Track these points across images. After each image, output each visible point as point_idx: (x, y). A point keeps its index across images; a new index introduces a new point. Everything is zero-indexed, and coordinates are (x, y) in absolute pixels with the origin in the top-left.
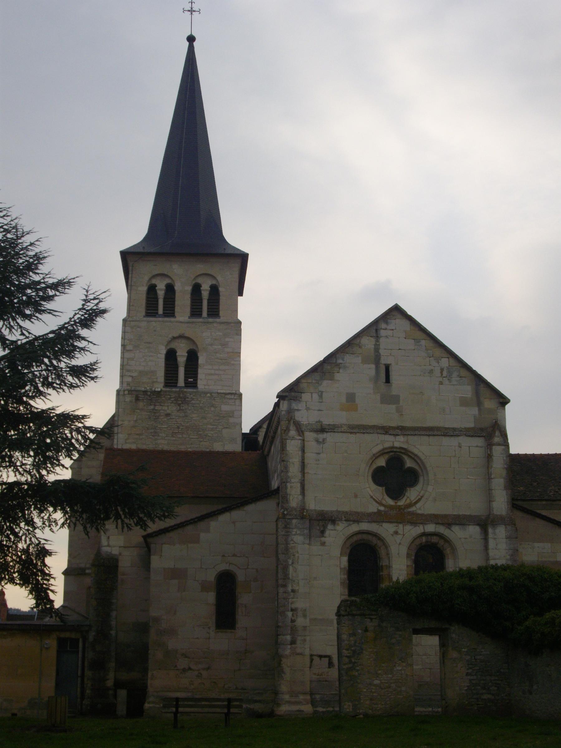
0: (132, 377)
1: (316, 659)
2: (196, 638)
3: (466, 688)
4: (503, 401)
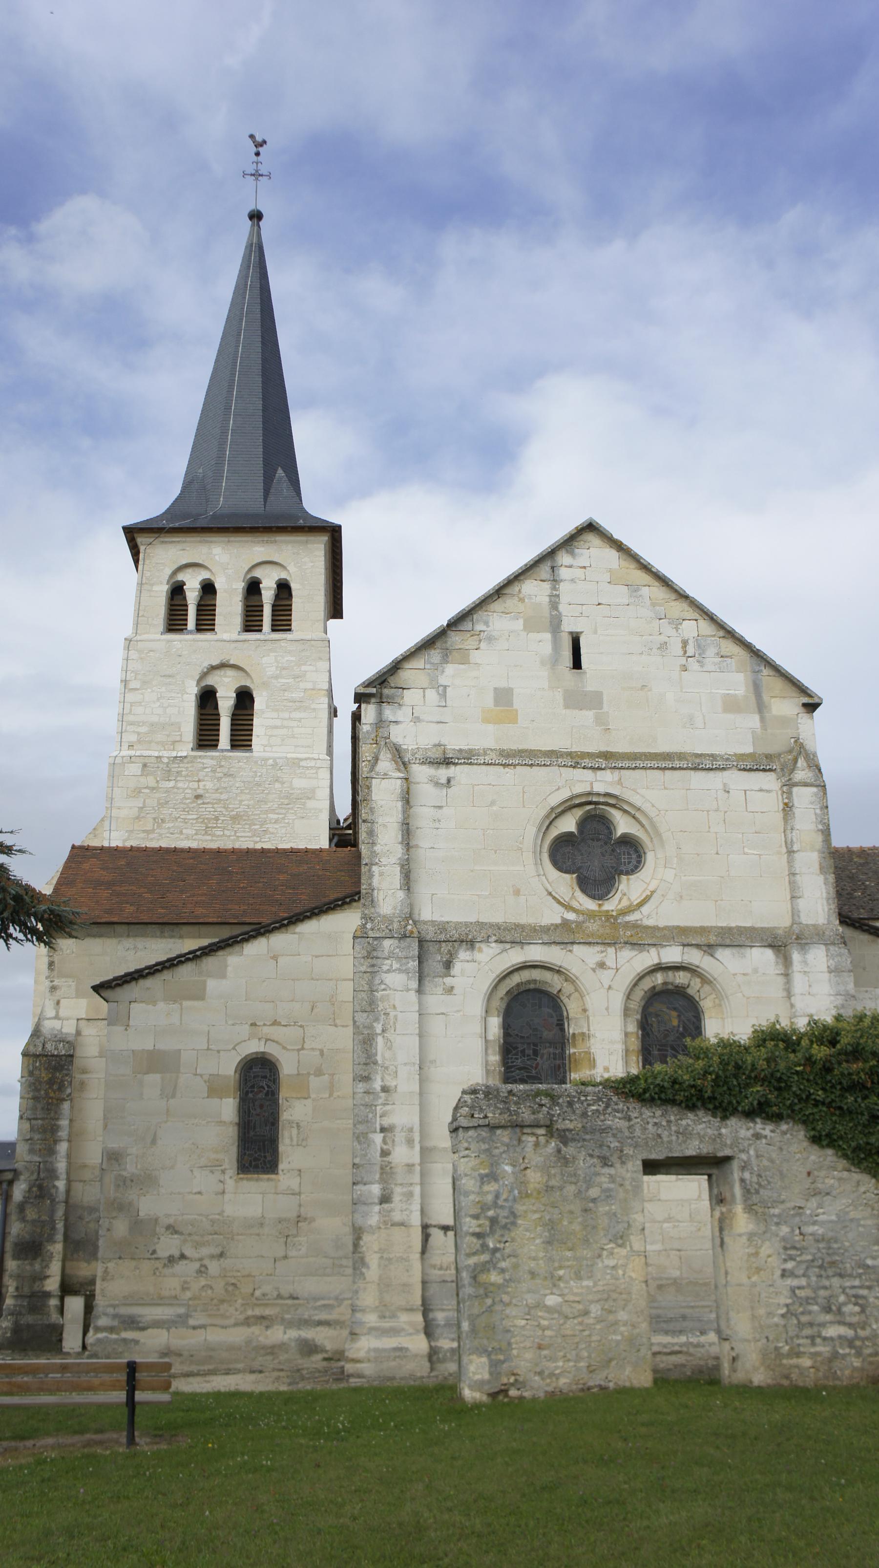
0: (139, 734)
2: (196, 1193)
3: (783, 1311)
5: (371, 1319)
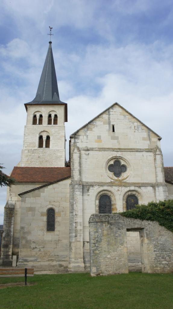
0: (27, 145)
3: (154, 258)
5: (73, 260)
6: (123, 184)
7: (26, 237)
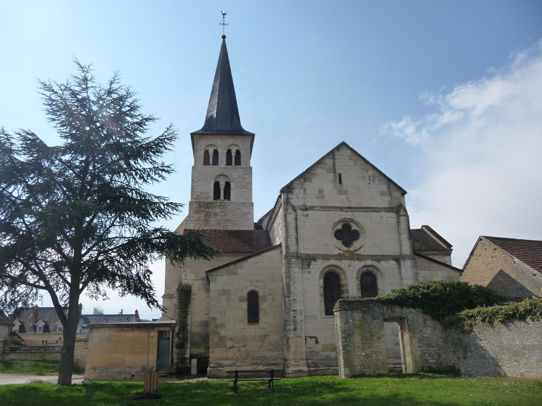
0: (197, 195)
1: (308, 339)
3: (419, 356)
4: (404, 193)
5: (292, 362)
6: (354, 256)
7: (219, 332)
